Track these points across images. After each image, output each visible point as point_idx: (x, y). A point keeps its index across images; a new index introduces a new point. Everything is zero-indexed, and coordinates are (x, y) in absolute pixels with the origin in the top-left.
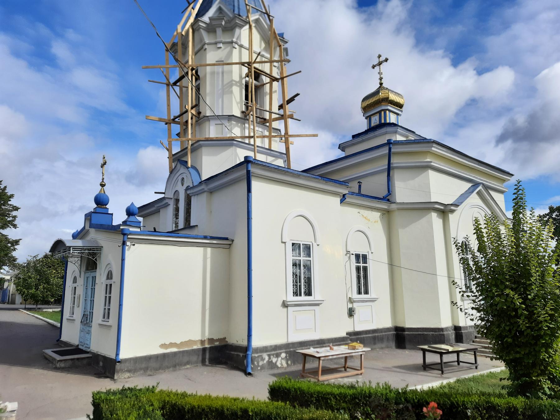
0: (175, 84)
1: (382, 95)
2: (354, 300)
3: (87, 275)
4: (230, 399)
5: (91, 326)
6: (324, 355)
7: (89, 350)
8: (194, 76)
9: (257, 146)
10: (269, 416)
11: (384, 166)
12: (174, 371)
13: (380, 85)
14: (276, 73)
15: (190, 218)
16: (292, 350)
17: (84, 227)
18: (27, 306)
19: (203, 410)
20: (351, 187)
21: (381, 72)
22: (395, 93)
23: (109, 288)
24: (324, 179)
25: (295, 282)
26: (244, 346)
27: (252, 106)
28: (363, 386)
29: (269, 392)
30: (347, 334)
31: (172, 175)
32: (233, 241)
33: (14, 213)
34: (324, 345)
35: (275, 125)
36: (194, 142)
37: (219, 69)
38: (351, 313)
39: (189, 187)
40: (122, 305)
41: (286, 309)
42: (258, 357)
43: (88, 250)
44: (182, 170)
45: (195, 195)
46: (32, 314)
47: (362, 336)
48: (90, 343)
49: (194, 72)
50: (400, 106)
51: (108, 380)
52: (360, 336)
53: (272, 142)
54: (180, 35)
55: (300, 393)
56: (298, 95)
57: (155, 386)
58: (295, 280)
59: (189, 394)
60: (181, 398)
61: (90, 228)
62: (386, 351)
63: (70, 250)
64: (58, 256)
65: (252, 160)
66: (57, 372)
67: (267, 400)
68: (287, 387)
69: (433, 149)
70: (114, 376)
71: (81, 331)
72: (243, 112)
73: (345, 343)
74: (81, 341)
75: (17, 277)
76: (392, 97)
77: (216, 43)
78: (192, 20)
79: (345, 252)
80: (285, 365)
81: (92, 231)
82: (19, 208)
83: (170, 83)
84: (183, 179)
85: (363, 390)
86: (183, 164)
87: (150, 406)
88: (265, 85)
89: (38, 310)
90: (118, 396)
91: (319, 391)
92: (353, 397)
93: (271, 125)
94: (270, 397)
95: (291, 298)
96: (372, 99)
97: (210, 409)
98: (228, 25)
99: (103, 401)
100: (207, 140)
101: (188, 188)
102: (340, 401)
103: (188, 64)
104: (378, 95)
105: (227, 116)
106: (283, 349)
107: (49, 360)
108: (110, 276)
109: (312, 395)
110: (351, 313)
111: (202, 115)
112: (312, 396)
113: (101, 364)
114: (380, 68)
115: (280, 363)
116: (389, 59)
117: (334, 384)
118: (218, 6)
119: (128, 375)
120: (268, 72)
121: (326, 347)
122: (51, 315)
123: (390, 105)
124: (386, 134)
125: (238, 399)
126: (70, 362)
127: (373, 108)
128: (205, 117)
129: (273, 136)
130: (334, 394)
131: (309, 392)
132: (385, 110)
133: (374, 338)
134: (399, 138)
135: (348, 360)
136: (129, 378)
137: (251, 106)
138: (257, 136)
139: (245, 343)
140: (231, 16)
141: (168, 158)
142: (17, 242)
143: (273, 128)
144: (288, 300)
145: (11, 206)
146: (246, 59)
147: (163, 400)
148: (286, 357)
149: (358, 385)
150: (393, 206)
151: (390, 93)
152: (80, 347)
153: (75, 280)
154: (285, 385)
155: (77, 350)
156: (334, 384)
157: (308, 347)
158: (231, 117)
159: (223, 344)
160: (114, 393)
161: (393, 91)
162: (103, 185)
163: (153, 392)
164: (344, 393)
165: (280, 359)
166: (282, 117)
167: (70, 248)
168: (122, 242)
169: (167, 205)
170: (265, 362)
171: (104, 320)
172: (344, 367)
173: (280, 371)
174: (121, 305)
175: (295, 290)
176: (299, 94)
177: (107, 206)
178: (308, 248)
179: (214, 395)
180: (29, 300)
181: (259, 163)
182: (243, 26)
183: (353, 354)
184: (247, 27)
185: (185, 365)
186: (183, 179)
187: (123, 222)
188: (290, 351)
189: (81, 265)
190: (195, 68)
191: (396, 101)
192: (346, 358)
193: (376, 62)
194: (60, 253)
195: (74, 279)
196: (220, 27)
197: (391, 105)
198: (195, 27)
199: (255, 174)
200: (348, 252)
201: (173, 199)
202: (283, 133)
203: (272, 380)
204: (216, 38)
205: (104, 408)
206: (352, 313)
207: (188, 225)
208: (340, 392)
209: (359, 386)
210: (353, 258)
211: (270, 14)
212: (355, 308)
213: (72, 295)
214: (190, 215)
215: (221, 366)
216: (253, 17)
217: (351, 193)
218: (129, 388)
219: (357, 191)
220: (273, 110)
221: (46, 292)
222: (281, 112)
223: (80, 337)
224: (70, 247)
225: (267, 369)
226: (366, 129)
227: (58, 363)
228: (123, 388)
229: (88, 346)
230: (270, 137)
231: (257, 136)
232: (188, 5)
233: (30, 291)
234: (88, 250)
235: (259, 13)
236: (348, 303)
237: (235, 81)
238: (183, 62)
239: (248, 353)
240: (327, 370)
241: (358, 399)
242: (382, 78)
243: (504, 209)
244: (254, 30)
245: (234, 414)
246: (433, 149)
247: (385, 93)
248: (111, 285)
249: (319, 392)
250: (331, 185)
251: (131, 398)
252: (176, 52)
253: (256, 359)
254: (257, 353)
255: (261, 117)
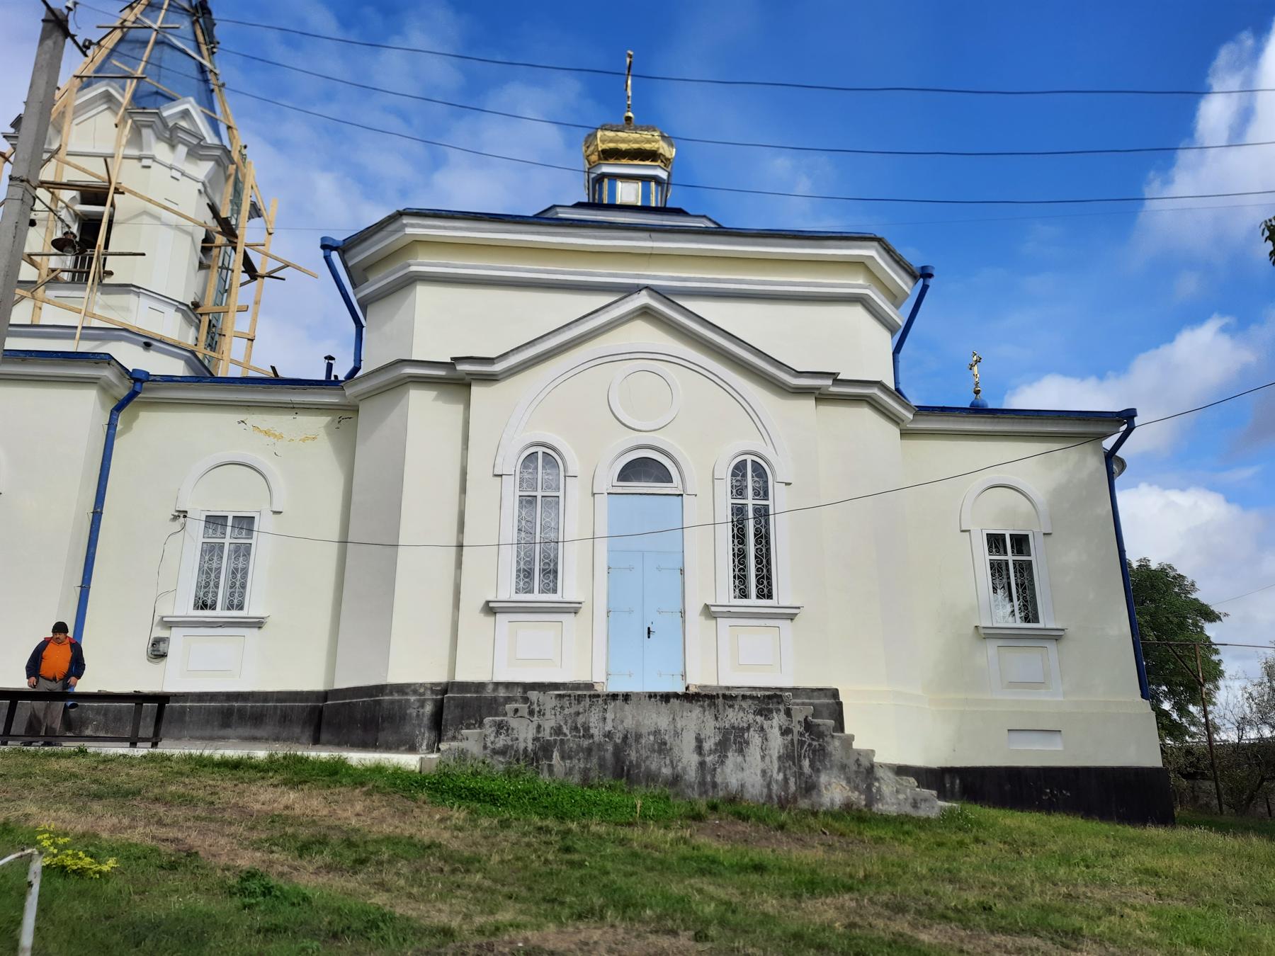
38: (158, 652)
41: (714, 621)
69: (409, 231)
77: (140, 159)
110: (158, 652)
162: (977, 392)
243: (1119, 435)
246: (409, 231)
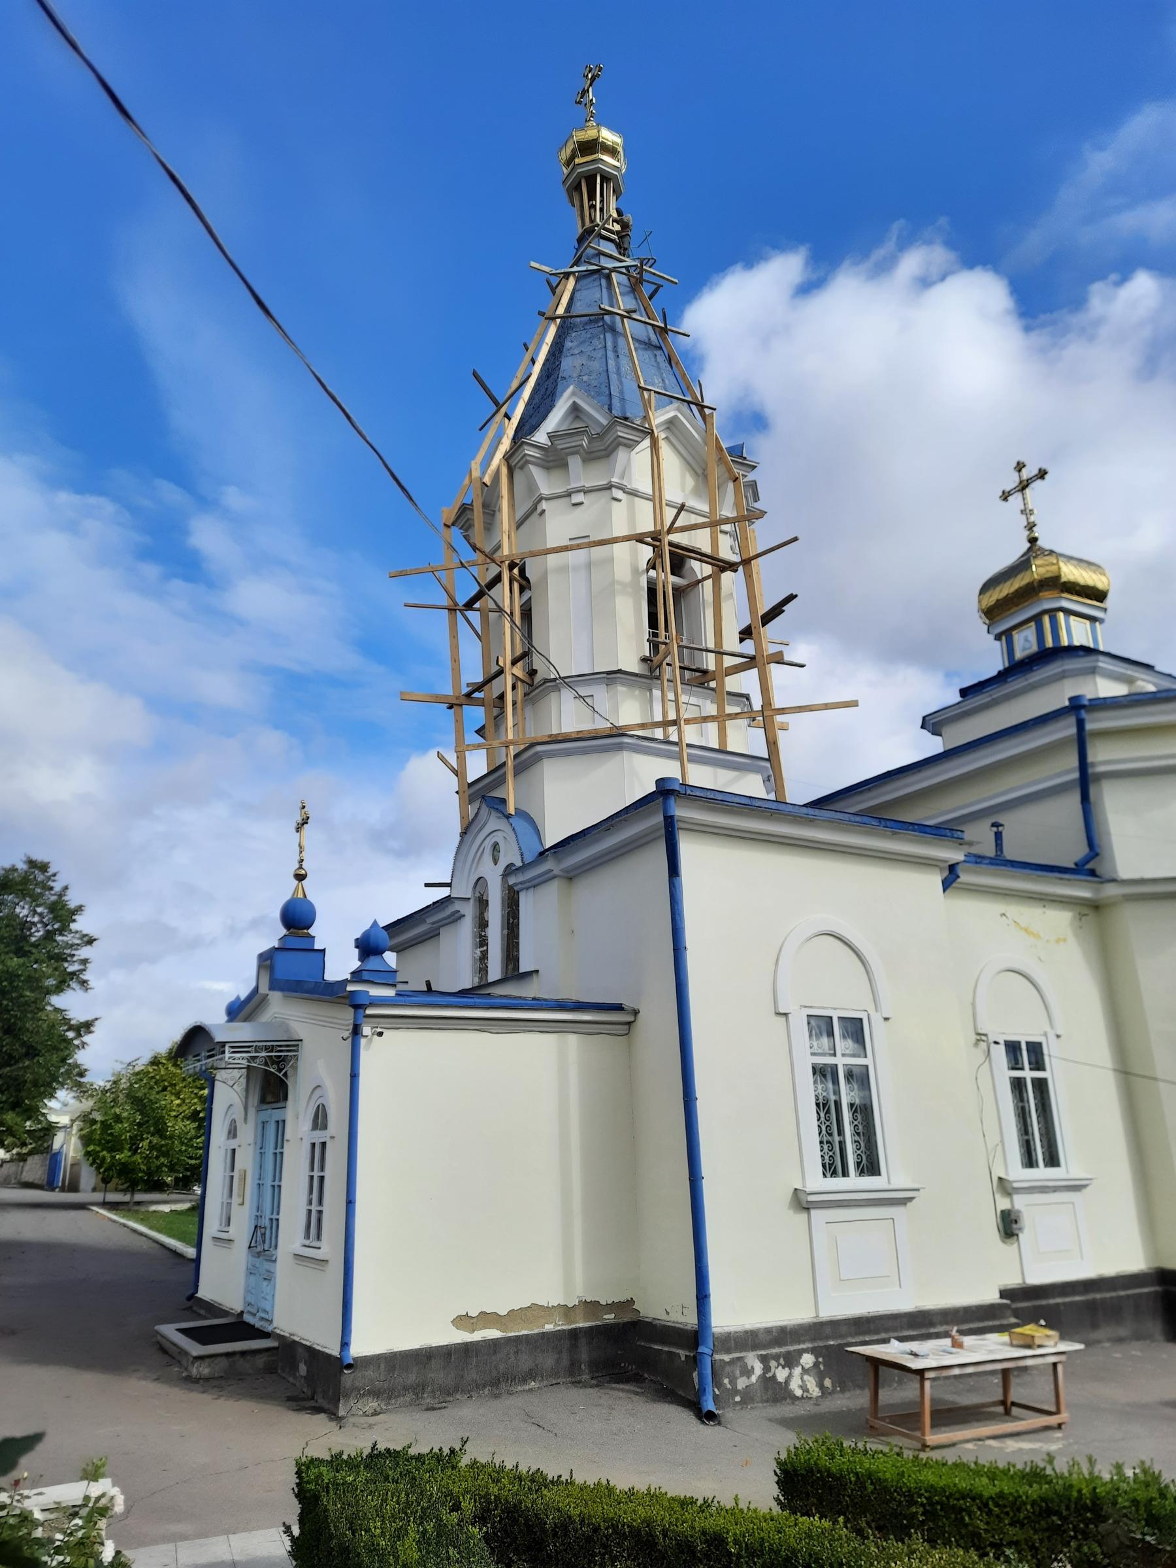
0: (469, 605)
1: (1039, 570)
2: (1016, 1185)
3: (264, 1115)
4: (669, 1500)
5: (274, 1259)
6: (934, 1364)
7: (269, 1329)
8: (517, 581)
9: (688, 745)
10: (787, 1559)
11: (1068, 772)
12: (496, 1396)
13: (1028, 545)
14: (727, 551)
15: (518, 951)
16: (832, 1343)
17: (256, 990)
18: (113, 1197)
19: (596, 1530)
20: (970, 844)
21: (1030, 507)
22: (1080, 561)
23: (318, 1153)
24: (888, 823)
25: (824, 1132)
26: (689, 1327)
27: (668, 641)
28: (1071, 1474)
29: (777, 1483)
30: (1004, 1293)
31: (468, 837)
32: (636, 1013)
33: (84, 952)
34: (932, 1330)
35: (733, 683)
36: (522, 747)
37: (577, 557)
38: (1009, 1226)
39: (513, 868)
40: (355, 1203)
41: (804, 1216)
42: (733, 1362)
43: (266, 1048)
44: (494, 822)
45: (527, 888)
46: (122, 1221)
47: (1052, 1301)
48: (273, 1306)
49: (516, 571)
50: (1099, 596)
51: (322, 1417)
52: (1044, 1302)
53: (729, 731)
54: (479, 485)
55: (875, 1489)
56: (791, 598)
57: (457, 1449)
58: (824, 1128)
59: (550, 1477)
60: (530, 1489)
61: (270, 989)
62: (1135, 1350)
63: (223, 1052)
64: (191, 1066)
65: (677, 787)
66: (192, 1391)
67: (776, 1510)
68: (834, 1470)
70: (337, 1408)
71: (250, 1273)
72: (645, 660)
73: (997, 1323)
74: (249, 1299)
75: (86, 1118)
76: (1070, 572)
77: (568, 494)
78: (505, 445)
79: (974, 1037)
80: (815, 1392)
81: (276, 997)
82: (95, 940)
83: (456, 604)
84: (495, 846)
85: (1071, 1486)
86: (496, 807)
87: (452, 1511)
88: (700, 584)
89: (136, 1208)
90: (365, 1474)
91: (932, 1486)
92: (1041, 1507)
93: (721, 684)
94: (782, 1498)
95: (817, 1182)
96: (1008, 583)
97: (614, 1527)
98: (598, 445)
99: (327, 1487)
100: (555, 740)
101: (509, 870)
102: (1001, 1520)
103: (500, 551)
104: (1029, 572)
105: (605, 675)
106: (804, 1342)
107: (170, 1355)
108: (320, 1120)
109: (910, 1497)
110: (1009, 1226)
111: (538, 678)
112: (912, 1502)
113: (303, 1369)
114: (1024, 499)
115: (800, 1383)
116: (1048, 470)
117: (976, 1463)
118: (571, 402)
119: (372, 1404)
120: (707, 549)
121: (938, 1336)
122: (168, 1223)
123: (1065, 595)
124: (1064, 677)
125: (693, 1502)
126: (224, 1362)
127: (1016, 608)
128: (547, 681)
129: (730, 715)
130: (980, 1496)
131: (901, 1488)
132: (1052, 612)
133: (1092, 1307)
134: (1107, 688)
135: (1014, 1381)
136: (375, 1414)
137: (666, 644)
138: (685, 720)
139: (690, 1319)
140: (604, 422)
141: (457, 792)
142: (86, 1027)
143: (729, 693)
144: (808, 1190)
145: (77, 935)
146: (646, 525)
147: (482, 1493)
148: (816, 1364)
149: (1053, 1469)
150: (1111, 891)
151: (1062, 564)
152: (247, 1318)
153: (233, 1133)
154: (825, 1461)
155: (240, 1328)
156: (976, 1463)
157: (883, 1336)
158: (613, 676)
159: (627, 1318)
160: (352, 1464)
161: (1070, 558)
162: (300, 877)
163: (454, 1468)
164: (1011, 1494)
165: (797, 1371)
166: (751, 662)
167: (224, 1046)
168: (351, 1027)
169: (457, 917)
170: (754, 1379)
171: (307, 1242)
172: (1003, 1403)
173: (800, 1410)
174: (350, 1203)
175: (827, 1157)
176: (796, 596)
177: (312, 931)
178: (855, 1029)
179: (621, 1482)
180: (115, 1181)
181: (698, 794)
182: (638, 443)
183: (1029, 1362)
184: (647, 442)
185: (524, 1381)
186: (495, 846)
187: (352, 973)
188: (828, 1347)
189: (247, 1090)
190: (518, 561)
191: (1082, 582)
192: (1005, 1373)
193: (1012, 481)
194: (199, 1061)
195: (231, 1125)
196: (577, 453)
197: (1070, 596)
198: (513, 462)
199: (688, 823)
200: (981, 1037)
201: (472, 901)
202: (757, 704)
203: (785, 1442)
204: (568, 480)
205: (330, 1507)
206: (1011, 1228)
207: (513, 971)
208: (998, 1490)
209: (1058, 1471)
210: (1000, 1053)
211: (705, 404)
212: (1019, 1212)
213: (225, 1172)
214: (516, 946)
215: (627, 1387)
216: (658, 418)
217: (973, 859)
218: (388, 1450)
219: (989, 850)
220: (727, 647)
221: (157, 1158)
222: (749, 647)
223: (248, 1291)
224: (223, 1044)
225: (762, 1401)
226: (1001, 668)
227: (193, 1363)
228: (373, 1449)
229: (267, 1317)
230: (721, 719)
231: (685, 720)
232: (495, 408)
233: (117, 1157)
234: (266, 1048)
235: (676, 404)
236: (998, 1196)
237: (620, 583)
238: (487, 550)
239: (701, 1349)
240: (950, 1410)
241: (1058, 1513)
242: (1035, 525)
244: (665, 450)
245: (685, 1547)
247: (1047, 565)
248: (324, 1144)
249: (932, 1489)
250: (910, 841)
251: (397, 1483)
252: (467, 527)
253: (728, 1369)
254: (728, 1351)
255: (694, 667)
